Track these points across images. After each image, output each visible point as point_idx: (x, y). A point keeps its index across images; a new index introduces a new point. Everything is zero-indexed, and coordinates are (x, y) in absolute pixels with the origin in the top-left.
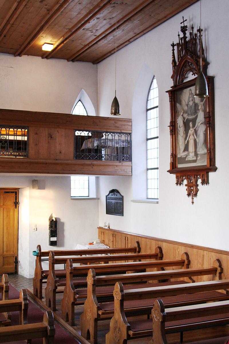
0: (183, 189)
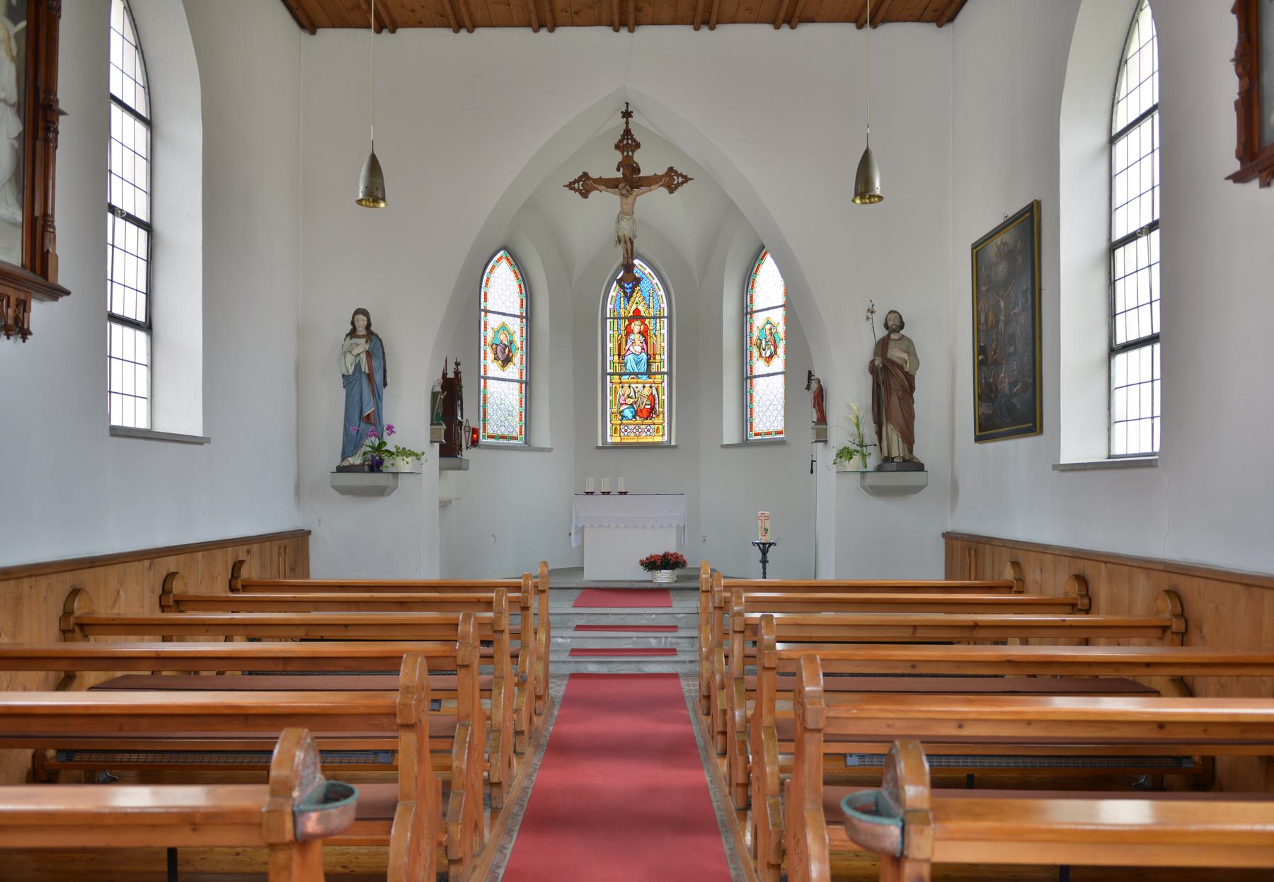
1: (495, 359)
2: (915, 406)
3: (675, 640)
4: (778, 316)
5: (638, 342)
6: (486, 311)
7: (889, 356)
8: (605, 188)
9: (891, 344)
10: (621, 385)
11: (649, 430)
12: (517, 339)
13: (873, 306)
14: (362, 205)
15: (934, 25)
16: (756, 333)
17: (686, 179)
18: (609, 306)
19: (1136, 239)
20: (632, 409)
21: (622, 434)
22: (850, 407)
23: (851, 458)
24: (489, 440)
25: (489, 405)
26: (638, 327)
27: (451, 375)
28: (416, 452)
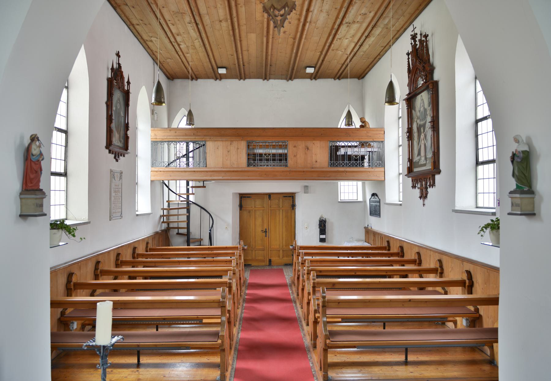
0: (417, 192)
19: (487, 119)
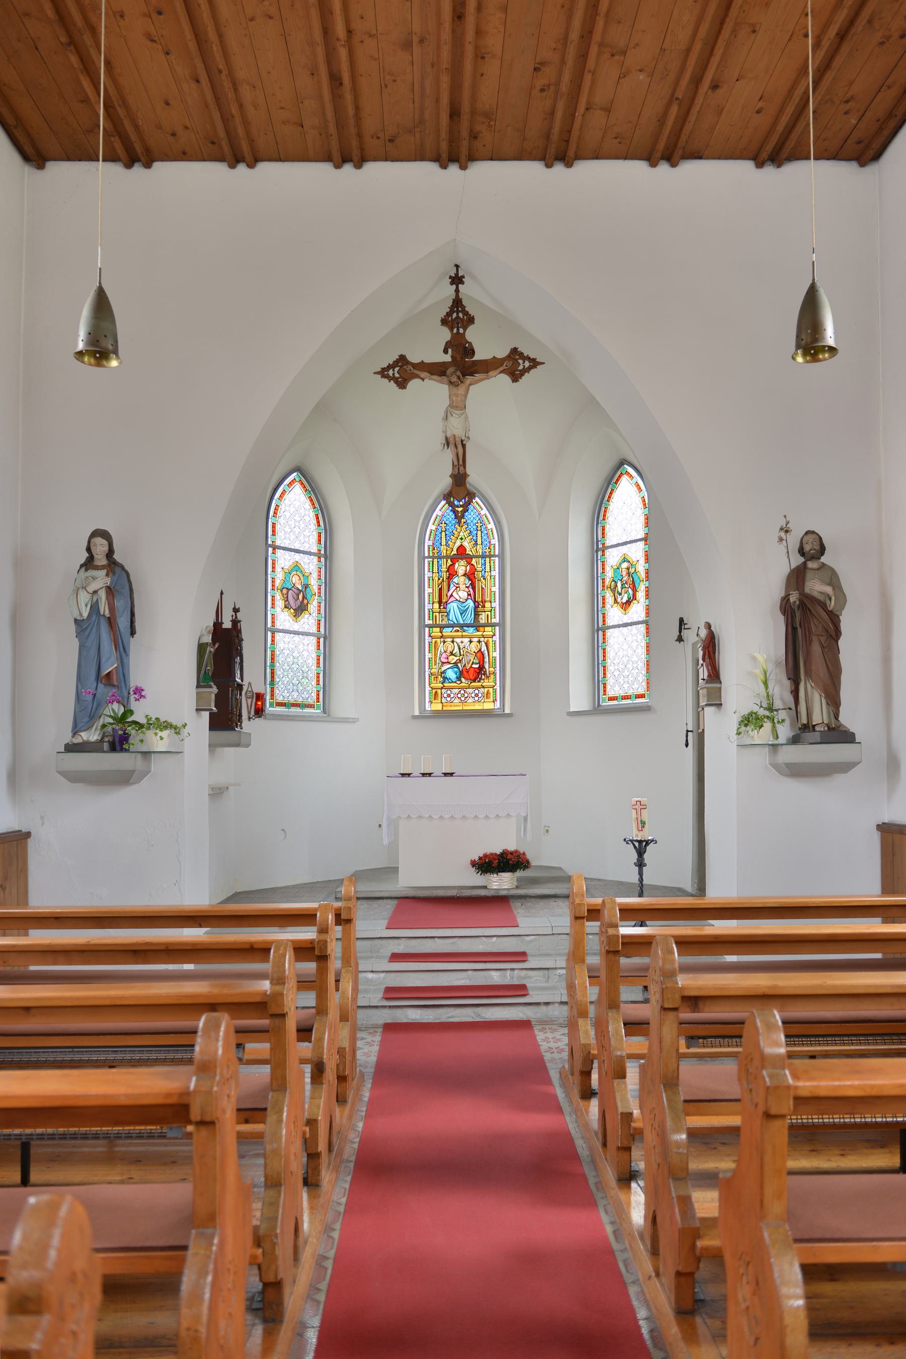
1: (286, 607)
2: (841, 656)
3: (524, 973)
4: (637, 552)
5: (462, 587)
6: (275, 548)
7: (807, 590)
8: (429, 375)
9: (809, 575)
10: (442, 640)
11: (477, 695)
12: (314, 582)
13: (788, 523)
14: (83, 362)
15: (854, 165)
16: (609, 574)
17: (535, 363)
18: (428, 543)
20: (456, 669)
21: (444, 700)
22: (754, 659)
23: (762, 726)
24: (279, 709)
25: (278, 664)
26: (463, 568)
27: (227, 624)
28: (174, 724)
